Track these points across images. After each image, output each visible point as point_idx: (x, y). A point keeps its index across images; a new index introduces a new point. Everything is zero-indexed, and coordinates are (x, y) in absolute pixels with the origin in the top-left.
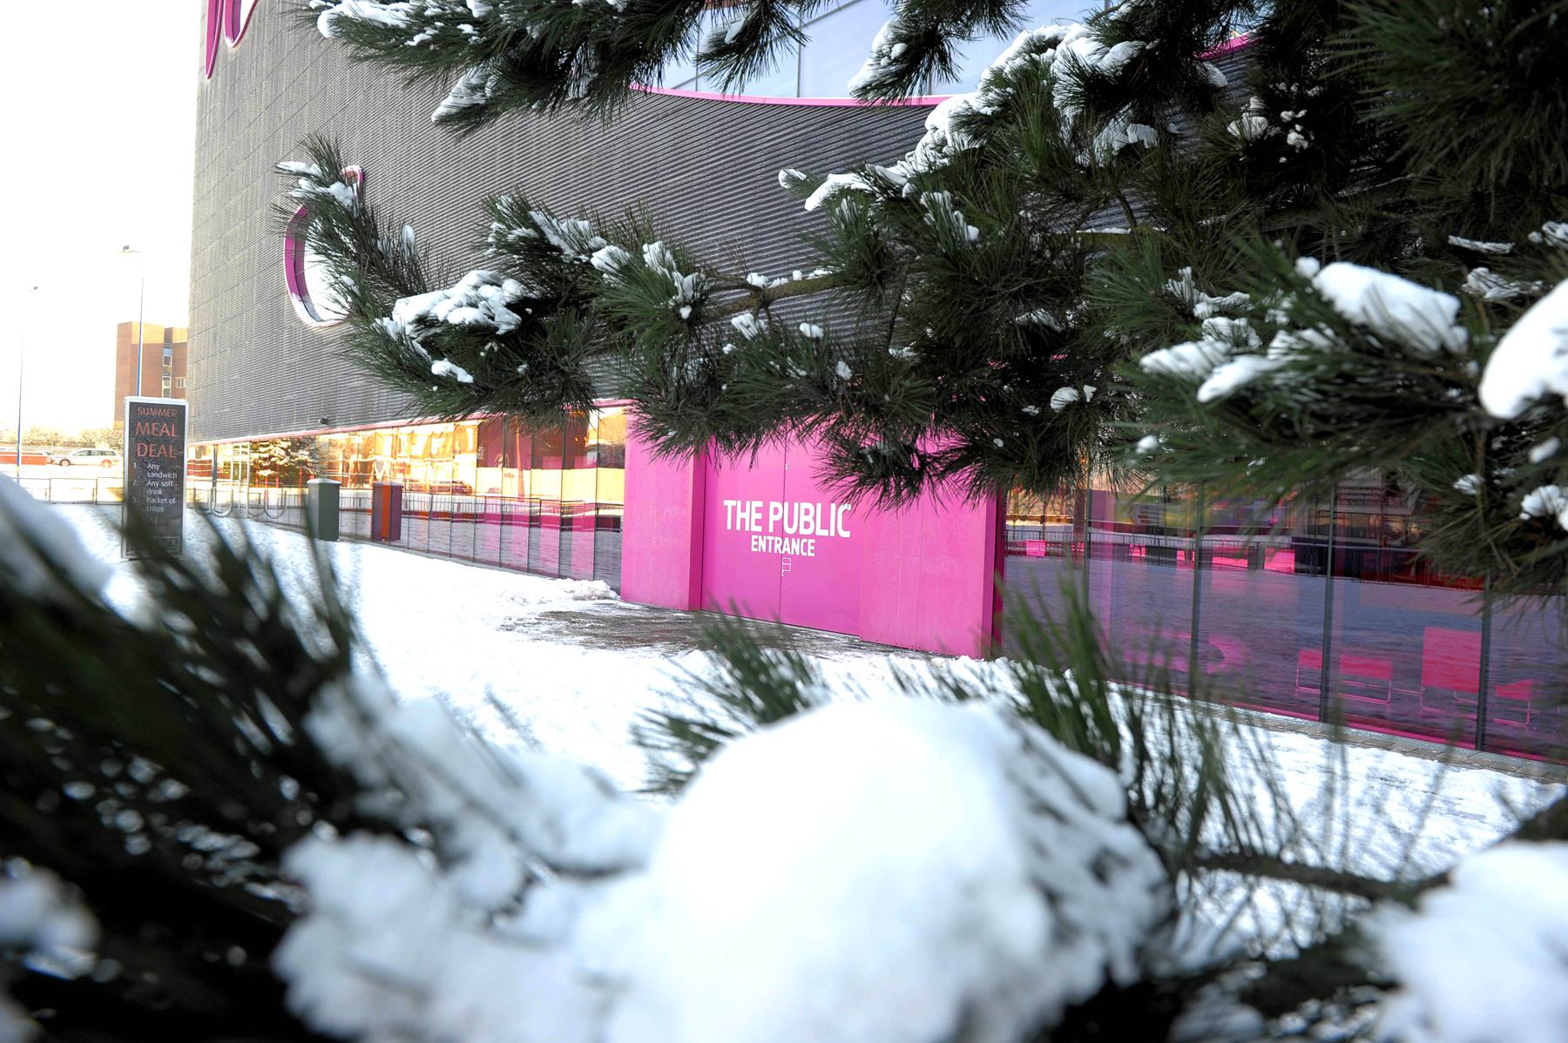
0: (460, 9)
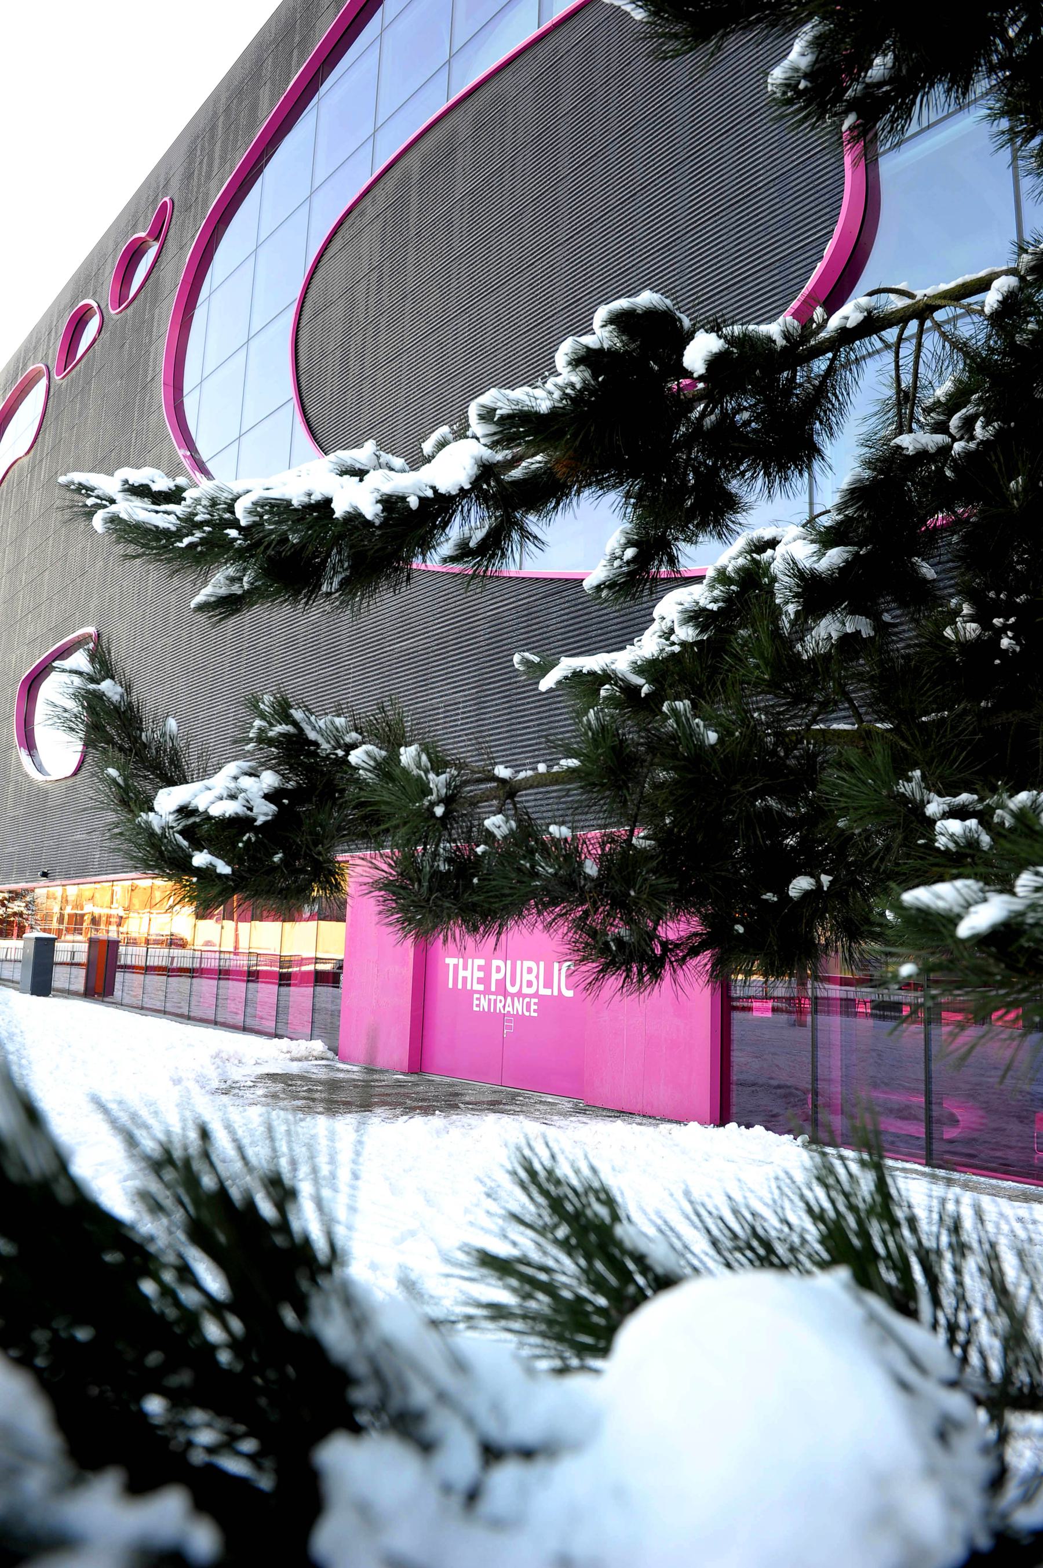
0: (227, 516)
